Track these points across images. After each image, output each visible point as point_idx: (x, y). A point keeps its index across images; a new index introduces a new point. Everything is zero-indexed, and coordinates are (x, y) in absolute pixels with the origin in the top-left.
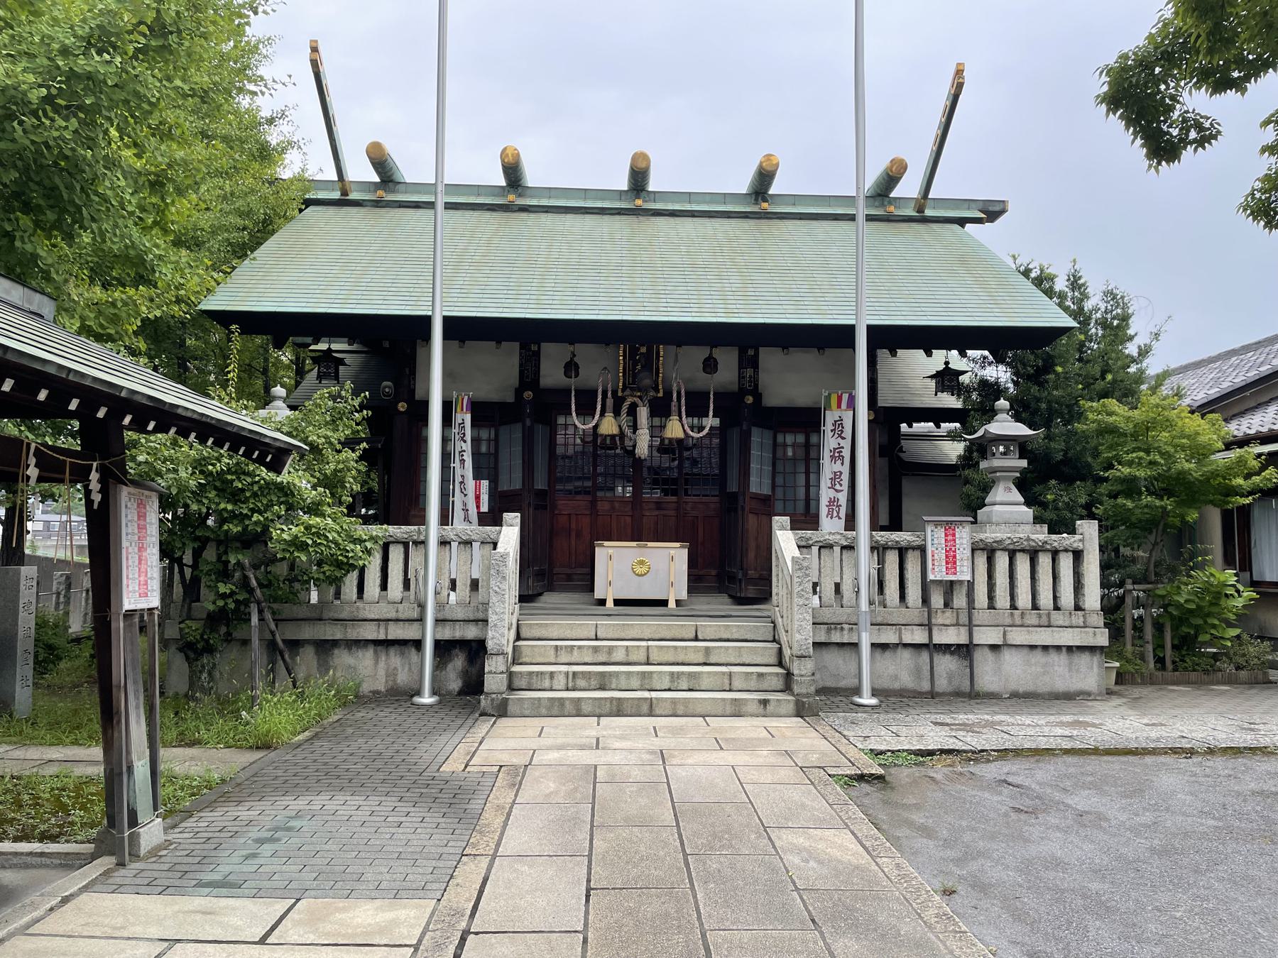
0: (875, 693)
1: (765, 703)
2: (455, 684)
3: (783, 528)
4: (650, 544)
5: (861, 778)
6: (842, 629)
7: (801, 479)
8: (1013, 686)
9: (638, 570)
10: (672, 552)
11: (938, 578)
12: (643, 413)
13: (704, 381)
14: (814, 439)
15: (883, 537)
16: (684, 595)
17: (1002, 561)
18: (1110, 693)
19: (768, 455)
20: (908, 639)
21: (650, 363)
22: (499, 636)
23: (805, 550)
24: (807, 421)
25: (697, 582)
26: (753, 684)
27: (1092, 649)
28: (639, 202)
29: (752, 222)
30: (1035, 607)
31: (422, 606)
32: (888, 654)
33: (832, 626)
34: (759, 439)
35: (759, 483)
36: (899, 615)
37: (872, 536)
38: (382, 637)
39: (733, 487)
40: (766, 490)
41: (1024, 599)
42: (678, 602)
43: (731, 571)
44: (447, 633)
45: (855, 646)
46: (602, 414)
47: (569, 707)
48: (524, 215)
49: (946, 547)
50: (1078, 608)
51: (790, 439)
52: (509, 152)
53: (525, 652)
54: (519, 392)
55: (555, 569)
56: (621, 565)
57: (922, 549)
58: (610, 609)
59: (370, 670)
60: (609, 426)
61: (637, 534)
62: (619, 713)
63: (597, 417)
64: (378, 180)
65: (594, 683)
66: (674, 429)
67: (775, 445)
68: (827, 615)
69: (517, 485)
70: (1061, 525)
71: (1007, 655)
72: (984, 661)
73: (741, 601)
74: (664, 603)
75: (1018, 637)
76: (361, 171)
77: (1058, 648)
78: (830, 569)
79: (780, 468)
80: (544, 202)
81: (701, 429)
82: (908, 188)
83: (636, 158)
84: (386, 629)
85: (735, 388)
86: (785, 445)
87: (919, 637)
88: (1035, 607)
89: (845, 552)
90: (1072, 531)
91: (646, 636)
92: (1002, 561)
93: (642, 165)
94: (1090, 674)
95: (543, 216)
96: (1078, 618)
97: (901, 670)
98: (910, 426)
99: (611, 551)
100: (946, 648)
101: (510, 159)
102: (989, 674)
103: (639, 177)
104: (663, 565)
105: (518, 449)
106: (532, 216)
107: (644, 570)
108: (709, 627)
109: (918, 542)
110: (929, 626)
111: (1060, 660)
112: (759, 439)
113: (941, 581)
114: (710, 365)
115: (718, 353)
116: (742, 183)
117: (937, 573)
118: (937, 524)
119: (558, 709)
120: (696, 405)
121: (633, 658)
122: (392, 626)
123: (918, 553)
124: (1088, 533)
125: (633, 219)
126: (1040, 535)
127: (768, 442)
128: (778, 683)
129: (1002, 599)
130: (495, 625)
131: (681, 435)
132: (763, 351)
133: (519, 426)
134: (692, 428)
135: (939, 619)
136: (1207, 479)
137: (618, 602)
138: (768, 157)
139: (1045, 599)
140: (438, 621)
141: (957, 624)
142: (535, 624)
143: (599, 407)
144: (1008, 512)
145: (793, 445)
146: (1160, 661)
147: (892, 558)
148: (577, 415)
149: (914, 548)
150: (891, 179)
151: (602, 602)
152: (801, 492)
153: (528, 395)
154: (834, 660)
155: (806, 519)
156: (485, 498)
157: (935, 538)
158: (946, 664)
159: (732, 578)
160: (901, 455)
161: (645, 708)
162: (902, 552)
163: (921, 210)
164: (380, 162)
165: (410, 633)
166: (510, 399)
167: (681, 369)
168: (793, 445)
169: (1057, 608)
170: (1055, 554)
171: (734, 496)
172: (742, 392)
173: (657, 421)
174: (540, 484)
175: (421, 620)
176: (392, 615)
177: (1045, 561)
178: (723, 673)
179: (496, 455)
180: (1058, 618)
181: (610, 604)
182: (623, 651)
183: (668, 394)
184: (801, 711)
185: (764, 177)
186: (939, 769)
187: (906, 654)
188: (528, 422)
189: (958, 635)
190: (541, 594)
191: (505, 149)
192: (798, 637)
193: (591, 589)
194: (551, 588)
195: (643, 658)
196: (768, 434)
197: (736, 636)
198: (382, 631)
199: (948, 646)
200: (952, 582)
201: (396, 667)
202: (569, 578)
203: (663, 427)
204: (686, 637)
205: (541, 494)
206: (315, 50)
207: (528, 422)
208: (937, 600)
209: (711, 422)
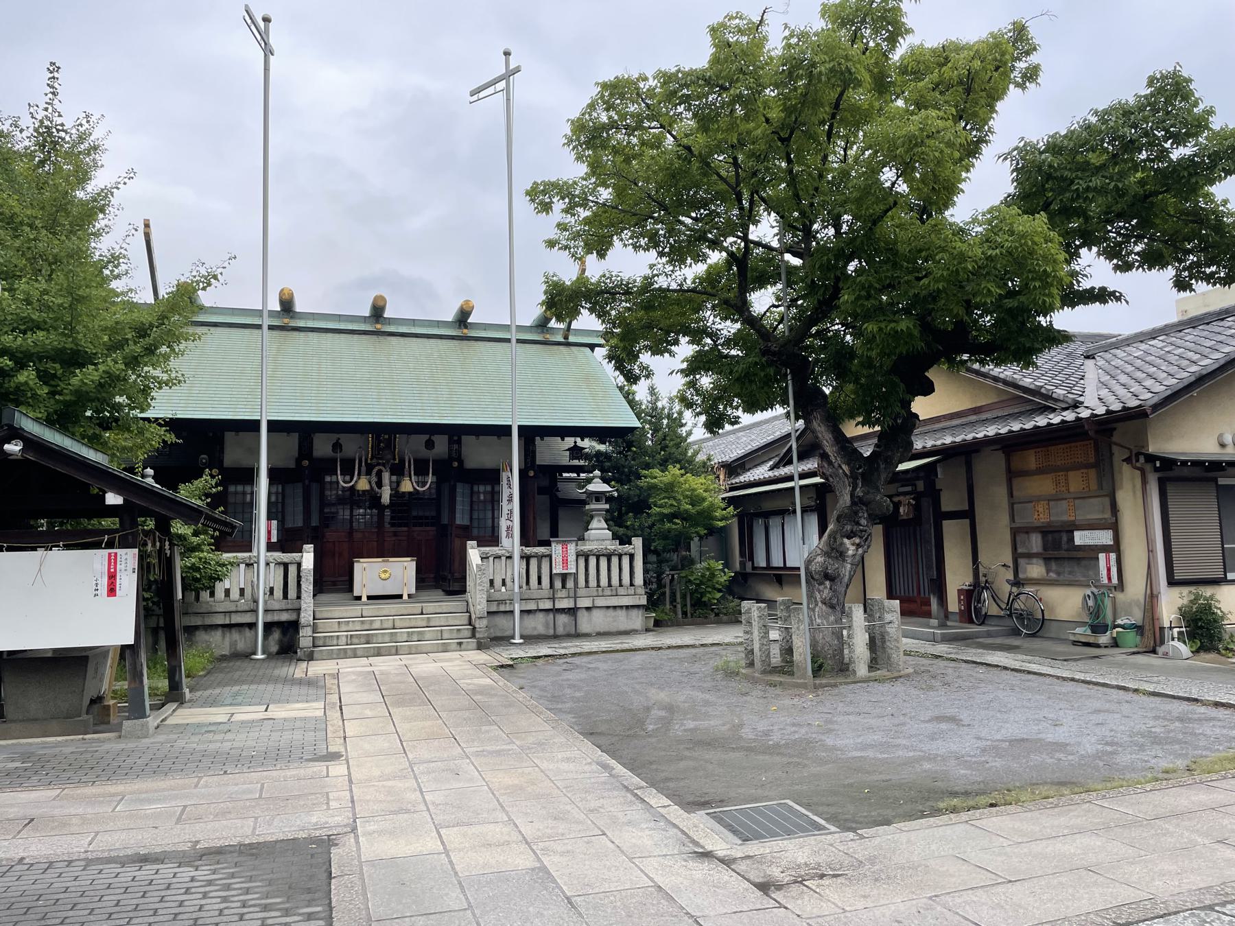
0: (522, 637)
1: (460, 644)
2: (274, 648)
5: (502, 666)
7: (489, 514)
8: (598, 629)
9: (383, 576)
12: (386, 476)
13: (424, 453)
14: (496, 489)
15: (529, 550)
16: (413, 591)
17: (593, 561)
18: (647, 630)
19: (467, 500)
20: (542, 606)
21: (390, 445)
22: (306, 617)
24: (492, 477)
25: (423, 581)
26: (455, 635)
27: (638, 607)
28: (379, 326)
30: (610, 585)
31: (256, 601)
33: (500, 602)
34: (461, 490)
35: (461, 519)
36: (536, 594)
38: (227, 622)
39: (445, 521)
40: (466, 522)
41: (604, 582)
42: (409, 596)
43: (441, 575)
44: (270, 618)
45: (512, 612)
46: (359, 474)
47: (349, 653)
48: (296, 334)
49: (563, 555)
50: (632, 585)
51: (482, 488)
54: (298, 461)
55: (334, 579)
56: (370, 574)
57: (550, 556)
59: (220, 643)
60: (363, 484)
61: (382, 552)
62: (379, 655)
65: (363, 640)
66: (407, 486)
67: (472, 493)
68: (497, 596)
69: (300, 524)
70: (625, 541)
71: (595, 612)
72: (583, 617)
73: (450, 593)
74: (400, 596)
75: (600, 602)
77: (621, 607)
78: (498, 571)
79: (476, 507)
80: (310, 324)
81: (424, 484)
83: (376, 298)
85: (446, 456)
86: (479, 492)
87: (548, 605)
88: (610, 585)
90: (630, 543)
92: (593, 561)
93: (380, 303)
94: (637, 620)
95: (310, 334)
96: (631, 590)
97: (538, 624)
100: (562, 611)
101: (286, 297)
102: (586, 623)
104: (400, 572)
105: (299, 500)
106: (302, 334)
108: (430, 607)
110: (553, 599)
111: (622, 614)
112: (461, 490)
114: (430, 445)
115: (436, 438)
116: (450, 316)
117: (558, 569)
118: (558, 542)
119: (343, 655)
120: (421, 468)
121: (385, 626)
122: (233, 616)
124: (638, 542)
125: (374, 337)
126: (614, 546)
127: (467, 491)
128: (468, 634)
129: (593, 582)
131: (411, 490)
132: (463, 437)
133: (300, 485)
134: (418, 483)
135: (559, 595)
136: (699, 513)
137: (369, 598)
138: (467, 302)
139: (615, 581)
140: (266, 611)
142: (324, 611)
144: (599, 533)
145: (484, 493)
146: (685, 613)
152: (489, 522)
153: (306, 463)
154: (501, 621)
155: (490, 538)
156: (274, 533)
158: (563, 619)
159: (444, 579)
161: (394, 651)
163: (566, 337)
165: (247, 619)
166: (292, 465)
167: (411, 448)
168: (484, 493)
169: (621, 585)
170: (620, 556)
171: (445, 527)
172: (451, 459)
173: (394, 478)
174: (315, 522)
175: (255, 611)
176: (234, 609)
177: (615, 560)
179: (283, 503)
180: (621, 591)
181: (364, 599)
183: (402, 461)
184: (480, 647)
186: (541, 661)
187: (541, 616)
188: (307, 482)
193: (351, 589)
195: (391, 625)
196: (467, 486)
199: (563, 609)
201: (240, 641)
202: (334, 583)
203: (398, 483)
205: (315, 529)
206: (147, 226)
207: (307, 482)
208: (558, 584)
209: (430, 479)
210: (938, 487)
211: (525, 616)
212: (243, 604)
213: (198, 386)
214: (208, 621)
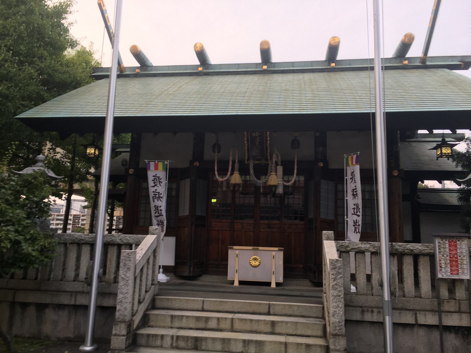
3: (328, 239)
4: (260, 248)
6: (372, 312)
9: (254, 263)
10: (274, 253)
11: (445, 277)
15: (400, 246)
16: (281, 280)
20: (422, 320)
23: (344, 255)
25: (289, 270)
29: (325, 74)
32: (408, 330)
37: (392, 246)
38: (73, 303)
39: (311, 216)
42: (278, 284)
45: (382, 324)
46: (233, 170)
52: (198, 45)
53: (152, 318)
54: (192, 162)
57: (432, 257)
58: (236, 287)
63: (229, 174)
64: (139, 65)
69: (187, 213)
76: (130, 62)
82: (415, 52)
83: (262, 44)
84: (76, 298)
87: (432, 320)
89: (373, 256)
91: (235, 310)
93: (266, 47)
98: (423, 182)
99: (237, 252)
101: (198, 49)
103: (265, 53)
107: (257, 263)
109: (427, 251)
110: (439, 312)
113: (445, 279)
116: (322, 56)
117: (444, 273)
121: (222, 326)
123: (427, 259)
130: (121, 302)
135: (446, 307)
137: (241, 283)
141: (459, 312)
143: (230, 168)
147: (408, 263)
148: (219, 175)
149: (424, 255)
150: (405, 46)
151: (232, 282)
153: (197, 164)
157: (441, 248)
160: (419, 200)
162: (416, 257)
164: (138, 55)
178: (281, 343)
182: (216, 321)
185: (333, 50)
187: (422, 332)
189: (461, 319)
190: (200, 276)
191: (196, 45)
192: (332, 320)
194: (204, 274)
197: (296, 313)
198: (73, 299)
200: (454, 280)
204: (262, 311)
210: (172, 240)
211: (400, 331)
212: (78, 286)
213: (103, 103)
214: (56, 300)
